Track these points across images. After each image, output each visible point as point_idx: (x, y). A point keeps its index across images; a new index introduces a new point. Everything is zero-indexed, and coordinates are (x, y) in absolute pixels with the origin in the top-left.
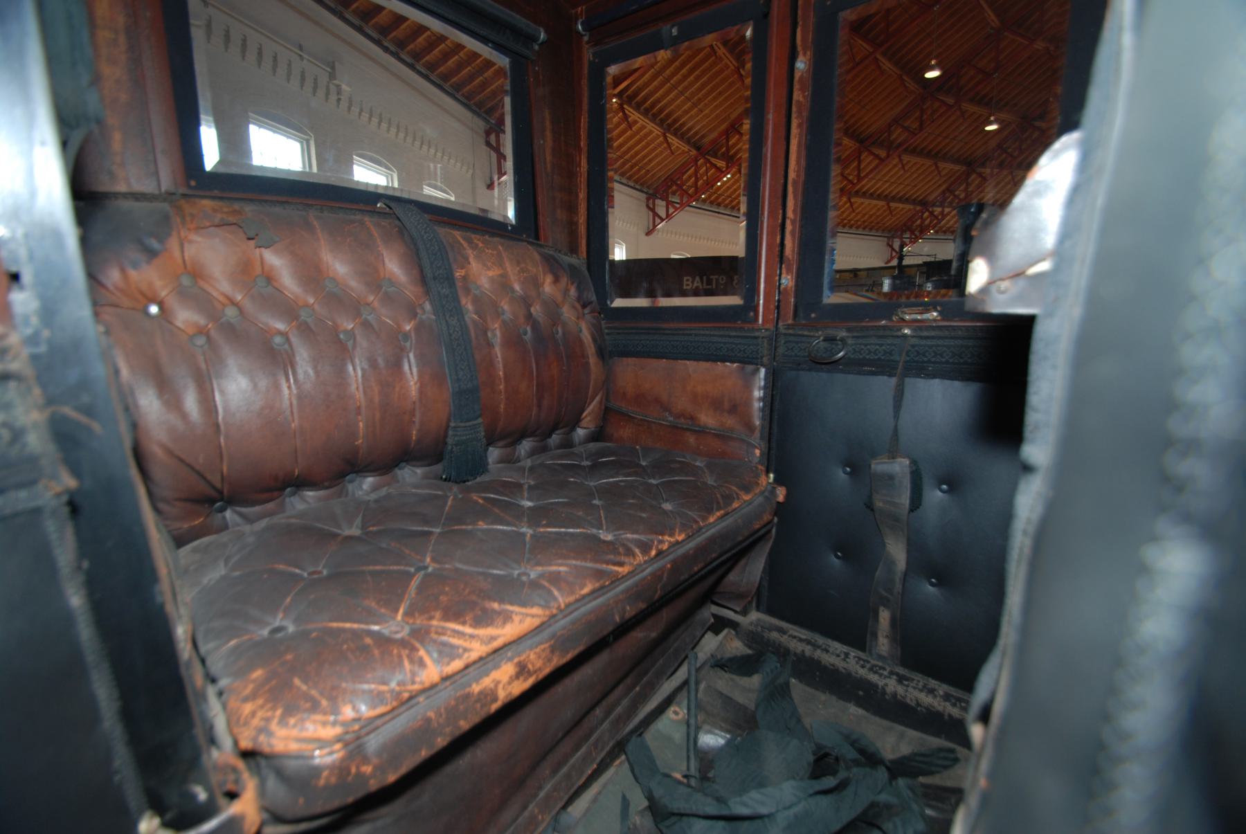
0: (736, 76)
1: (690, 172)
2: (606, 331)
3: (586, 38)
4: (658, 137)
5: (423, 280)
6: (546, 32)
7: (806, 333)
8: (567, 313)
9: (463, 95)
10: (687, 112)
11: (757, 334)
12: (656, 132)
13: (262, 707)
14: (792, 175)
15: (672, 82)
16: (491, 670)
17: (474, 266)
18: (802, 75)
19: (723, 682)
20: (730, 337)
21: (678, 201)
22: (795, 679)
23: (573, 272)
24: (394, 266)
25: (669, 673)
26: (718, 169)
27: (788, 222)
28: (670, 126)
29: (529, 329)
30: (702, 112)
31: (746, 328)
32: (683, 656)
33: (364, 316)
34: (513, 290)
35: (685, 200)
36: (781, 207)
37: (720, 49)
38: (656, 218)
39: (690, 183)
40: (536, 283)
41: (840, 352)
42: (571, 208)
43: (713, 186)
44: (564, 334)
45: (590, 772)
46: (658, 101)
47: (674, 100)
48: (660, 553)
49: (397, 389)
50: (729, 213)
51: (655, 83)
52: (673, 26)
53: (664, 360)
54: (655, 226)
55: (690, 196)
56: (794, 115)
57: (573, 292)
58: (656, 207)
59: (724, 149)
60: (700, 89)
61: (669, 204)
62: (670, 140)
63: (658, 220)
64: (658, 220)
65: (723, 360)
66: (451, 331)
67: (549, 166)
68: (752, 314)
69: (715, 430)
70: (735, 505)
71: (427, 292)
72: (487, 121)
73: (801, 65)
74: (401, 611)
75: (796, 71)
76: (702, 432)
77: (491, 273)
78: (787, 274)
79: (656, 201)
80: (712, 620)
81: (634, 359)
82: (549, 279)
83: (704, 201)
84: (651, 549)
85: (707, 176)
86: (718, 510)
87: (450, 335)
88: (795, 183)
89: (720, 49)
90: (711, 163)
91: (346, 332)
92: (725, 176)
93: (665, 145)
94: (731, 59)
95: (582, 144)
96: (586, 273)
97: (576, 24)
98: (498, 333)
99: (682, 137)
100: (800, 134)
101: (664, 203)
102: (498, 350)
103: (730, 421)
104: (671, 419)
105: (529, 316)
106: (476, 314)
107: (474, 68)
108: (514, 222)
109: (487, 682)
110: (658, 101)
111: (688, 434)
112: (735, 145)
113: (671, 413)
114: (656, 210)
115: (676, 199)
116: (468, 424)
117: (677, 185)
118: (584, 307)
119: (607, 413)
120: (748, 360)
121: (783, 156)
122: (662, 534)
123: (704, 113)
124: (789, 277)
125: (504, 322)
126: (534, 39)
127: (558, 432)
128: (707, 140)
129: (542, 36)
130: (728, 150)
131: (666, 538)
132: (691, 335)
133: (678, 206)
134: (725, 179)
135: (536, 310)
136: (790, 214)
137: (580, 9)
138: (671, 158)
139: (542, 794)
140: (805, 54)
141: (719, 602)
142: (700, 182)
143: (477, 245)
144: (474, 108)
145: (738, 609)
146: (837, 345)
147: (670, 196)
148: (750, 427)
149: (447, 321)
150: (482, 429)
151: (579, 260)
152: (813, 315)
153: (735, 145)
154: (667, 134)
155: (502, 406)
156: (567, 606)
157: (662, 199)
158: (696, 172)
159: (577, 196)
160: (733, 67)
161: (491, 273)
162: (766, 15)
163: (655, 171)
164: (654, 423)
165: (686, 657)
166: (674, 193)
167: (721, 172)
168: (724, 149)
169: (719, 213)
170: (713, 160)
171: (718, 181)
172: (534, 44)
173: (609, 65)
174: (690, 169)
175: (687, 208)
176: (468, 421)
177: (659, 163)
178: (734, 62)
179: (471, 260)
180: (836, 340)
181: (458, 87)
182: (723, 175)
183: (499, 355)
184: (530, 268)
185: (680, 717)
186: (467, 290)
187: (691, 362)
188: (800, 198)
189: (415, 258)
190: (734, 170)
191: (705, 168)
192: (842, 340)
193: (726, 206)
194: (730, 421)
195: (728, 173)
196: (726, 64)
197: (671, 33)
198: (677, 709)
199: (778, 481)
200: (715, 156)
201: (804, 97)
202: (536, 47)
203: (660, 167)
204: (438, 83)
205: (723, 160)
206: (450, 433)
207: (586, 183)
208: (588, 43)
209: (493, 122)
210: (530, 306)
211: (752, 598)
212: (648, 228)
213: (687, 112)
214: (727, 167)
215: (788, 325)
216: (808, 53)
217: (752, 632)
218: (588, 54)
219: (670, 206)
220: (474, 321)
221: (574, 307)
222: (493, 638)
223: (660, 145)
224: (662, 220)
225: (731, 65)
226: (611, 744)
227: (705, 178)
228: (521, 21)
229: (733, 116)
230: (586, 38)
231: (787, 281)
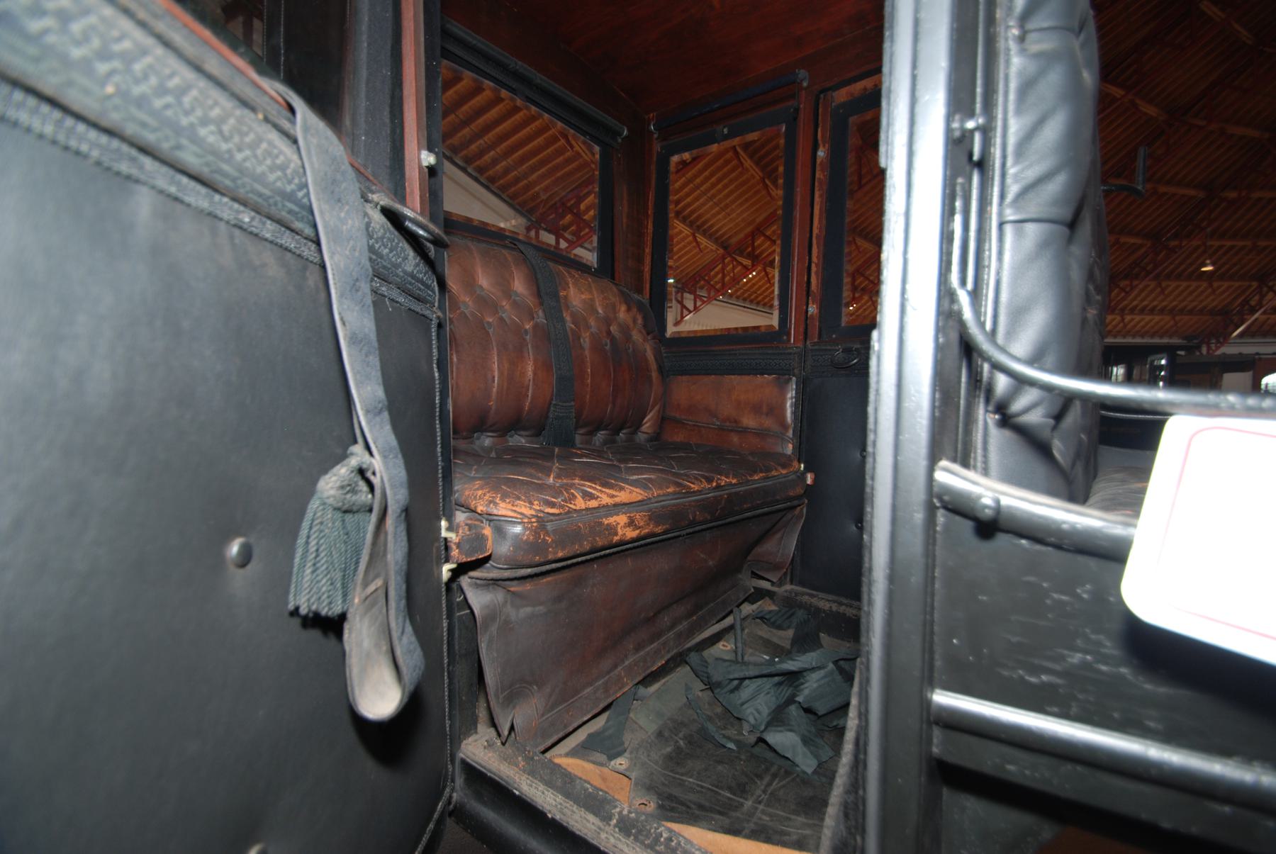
0: (761, 185)
1: (717, 270)
2: (665, 355)
3: (656, 136)
4: (688, 236)
5: (538, 294)
6: (628, 130)
7: (829, 348)
8: (637, 336)
9: (508, 196)
10: (714, 216)
11: (791, 351)
12: (686, 232)
13: (489, 492)
14: (815, 231)
15: (702, 189)
16: (614, 515)
17: (572, 291)
18: (822, 161)
19: (764, 631)
20: (768, 354)
21: (706, 295)
22: (824, 633)
23: (641, 307)
24: (519, 286)
25: (718, 618)
26: (745, 267)
27: (813, 265)
28: (699, 227)
29: (608, 341)
30: (729, 215)
31: (781, 347)
32: (729, 609)
33: (500, 314)
34: (598, 313)
35: (712, 293)
36: (807, 254)
37: (746, 161)
38: (684, 310)
39: (716, 279)
40: (614, 309)
41: (855, 359)
42: (640, 260)
43: (739, 282)
44: (634, 350)
45: (660, 665)
46: (689, 205)
47: (703, 204)
48: (718, 487)
49: (519, 368)
50: (755, 308)
51: (686, 190)
52: (724, 127)
53: (713, 376)
54: (682, 317)
55: (718, 291)
56: (816, 189)
57: (640, 321)
58: (684, 300)
59: (750, 249)
60: (728, 196)
61: (696, 297)
62: (699, 240)
63: (685, 312)
64: (685, 312)
65: (762, 374)
66: (557, 333)
67: (624, 225)
68: (785, 337)
69: (755, 429)
70: (774, 473)
71: (541, 304)
72: (529, 220)
73: (821, 153)
74: (552, 476)
75: (818, 157)
76: (744, 431)
77: (583, 297)
78: (813, 304)
79: (685, 294)
80: (752, 590)
81: (687, 376)
82: (623, 308)
83: (731, 295)
84: (712, 481)
85: (734, 272)
86: (761, 472)
87: (556, 335)
88: (818, 236)
89: (746, 161)
90: (736, 260)
91: (488, 322)
92: (751, 273)
93: (694, 244)
94: (757, 170)
95: (649, 212)
96: (650, 309)
97: (649, 125)
98: (587, 340)
99: (710, 237)
100: (821, 202)
101: (692, 297)
102: (587, 353)
103: (768, 422)
104: (719, 423)
105: (609, 333)
106: (573, 324)
107: (519, 173)
108: (596, 266)
109: (612, 520)
110: (689, 205)
111: (732, 434)
112: (759, 246)
113: (718, 419)
114: (684, 303)
115: (703, 293)
116: (564, 404)
117: (705, 280)
118: (648, 334)
119: (663, 420)
120: (783, 374)
121: (809, 222)
122: (721, 475)
123: (731, 217)
124: (815, 306)
125: (592, 334)
126: (620, 134)
127: (624, 431)
128: (734, 240)
129: (625, 132)
130: (754, 249)
131: (723, 478)
132: (735, 354)
133: (705, 299)
134: (750, 276)
135: (614, 329)
136: (814, 259)
137: (652, 115)
138: (699, 256)
139: (627, 663)
140: (824, 146)
141: (763, 575)
142: (727, 279)
143: (574, 276)
144: (518, 207)
145: (775, 581)
146: (853, 354)
147: (698, 290)
148: (784, 425)
149: (554, 325)
150: (573, 410)
151: (645, 299)
152: (834, 336)
153: (759, 246)
154: (697, 235)
155: (588, 397)
156: (658, 496)
157: (690, 293)
158: (723, 269)
159: (644, 251)
160: (758, 178)
161: (583, 297)
162: (795, 119)
163: (684, 267)
164: (704, 427)
165: (731, 612)
166: (702, 288)
167: (747, 270)
168: (750, 249)
169: (745, 307)
170: (739, 259)
171: (745, 278)
172: (618, 137)
173: (673, 155)
174: (718, 265)
175: (715, 302)
176: (564, 402)
177: (688, 260)
178: (760, 173)
179: (570, 285)
180: (853, 351)
181: (504, 188)
182: (748, 272)
183: (588, 357)
184: (611, 297)
185: (729, 648)
186: (567, 307)
187: (736, 376)
188: (822, 248)
189: (534, 279)
190: (759, 268)
191: (731, 266)
192: (856, 349)
193: (751, 301)
194: (768, 422)
195: (754, 271)
196: (752, 175)
197: (723, 132)
198: (725, 644)
199: (807, 469)
200: (741, 255)
201: (824, 176)
202: (620, 140)
203: (689, 264)
204: (486, 183)
205: (749, 259)
206: (552, 408)
207: (651, 242)
208: (657, 139)
209: (534, 219)
210: (610, 326)
211: (787, 569)
212: (676, 319)
213: (714, 216)
214: (753, 266)
215: (815, 343)
216: (827, 145)
217: (788, 597)
218: (657, 147)
219: (698, 300)
220: (572, 329)
221: (640, 332)
222: (613, 496)
223: (689, 243)
224: (690, 312)
225: (756, 175)
226: (675, 651)
227: (732, 275)
228: (612, 122)
229: (758, 220)
230: (656, 136)
231: (813, 309)
